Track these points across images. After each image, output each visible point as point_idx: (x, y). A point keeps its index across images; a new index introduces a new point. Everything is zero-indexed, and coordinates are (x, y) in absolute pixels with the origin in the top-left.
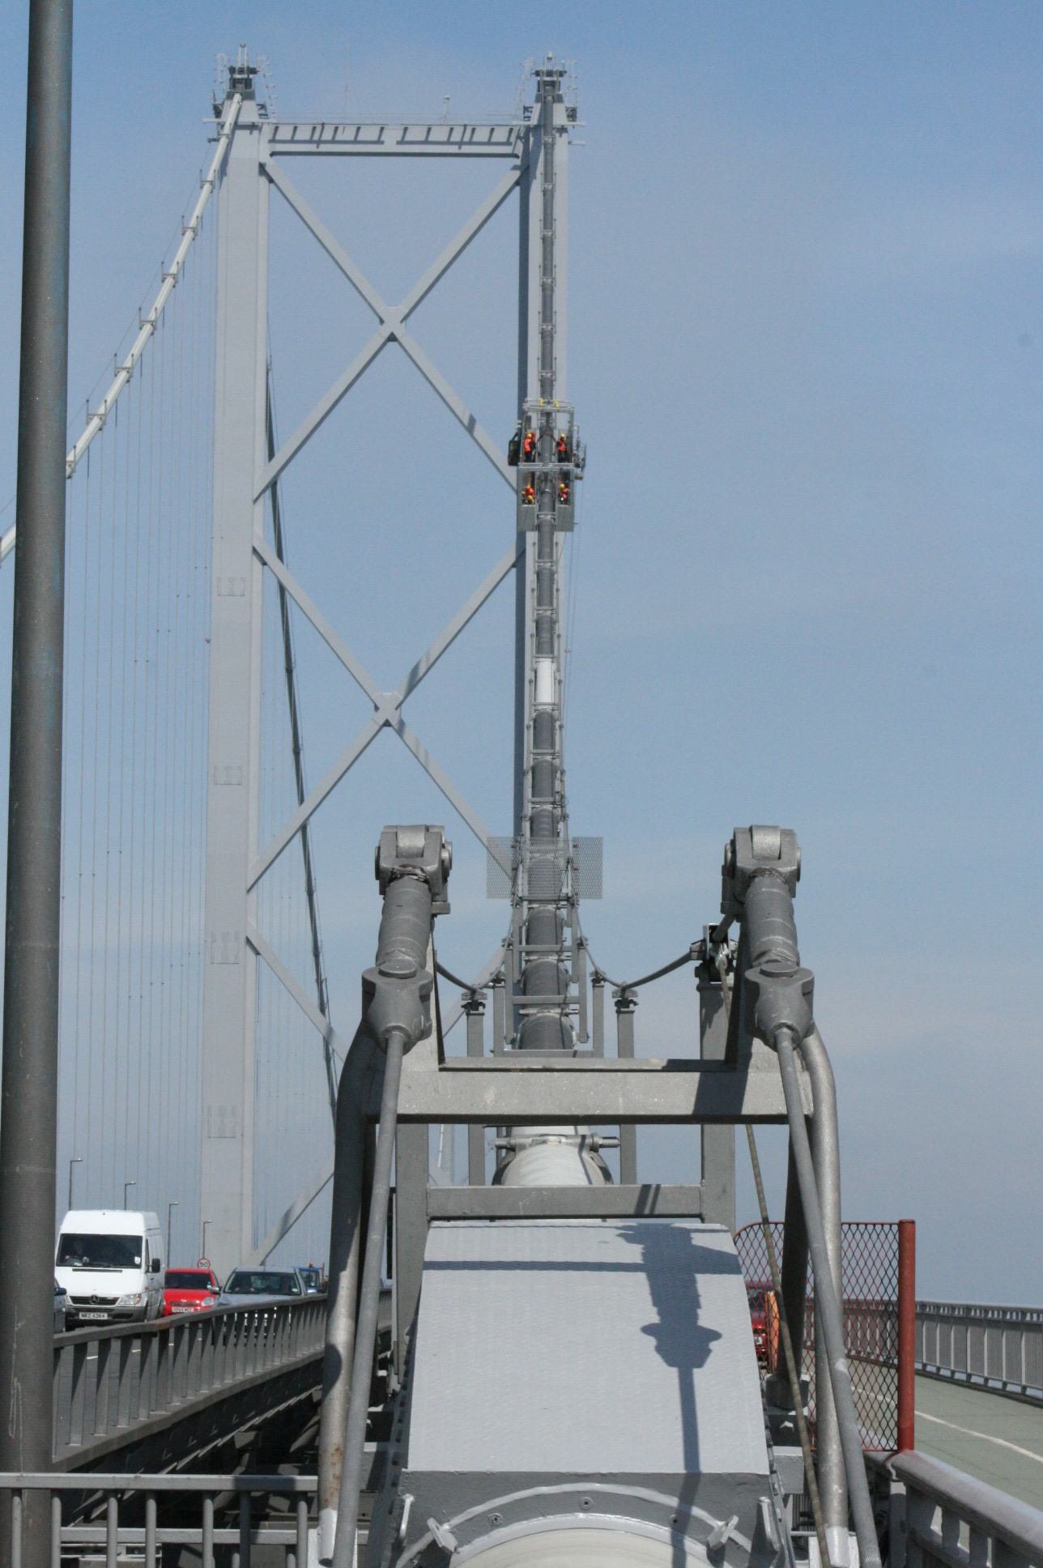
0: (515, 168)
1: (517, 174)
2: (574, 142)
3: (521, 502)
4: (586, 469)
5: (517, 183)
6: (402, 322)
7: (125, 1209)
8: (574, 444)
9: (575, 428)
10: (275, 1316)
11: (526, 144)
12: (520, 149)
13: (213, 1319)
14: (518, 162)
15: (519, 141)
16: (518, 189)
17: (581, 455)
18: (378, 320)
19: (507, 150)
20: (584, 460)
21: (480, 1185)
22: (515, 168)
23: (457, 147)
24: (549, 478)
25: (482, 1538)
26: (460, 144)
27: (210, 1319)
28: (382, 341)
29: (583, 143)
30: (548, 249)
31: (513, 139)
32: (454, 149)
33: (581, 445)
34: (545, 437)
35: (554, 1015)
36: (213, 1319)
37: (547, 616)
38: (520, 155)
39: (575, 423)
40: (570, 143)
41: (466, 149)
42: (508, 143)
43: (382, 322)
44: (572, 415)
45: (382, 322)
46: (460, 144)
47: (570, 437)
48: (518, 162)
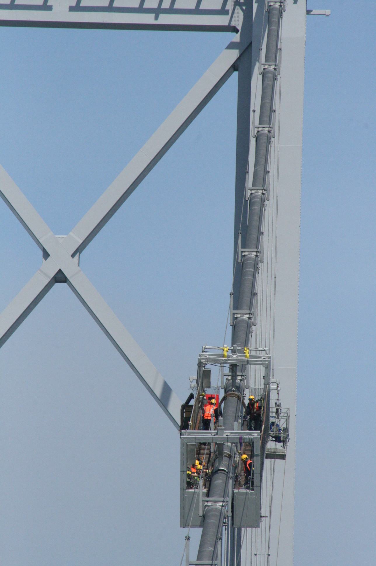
0: (232, 46)
1: (234, 54)
2: (314, 12)
3: (185, 485)
4: (289, 444)
5: (234, 67)
6: (73, 256)
7: (181, 471)
8: (273, 409)
9: (273, 386)
10: (186, 496)
11: (248, 14)
12: (238, 21)
13: (207, 443)
14: (236, 38)
15: (238, 8)
16: (236, 74)
17: (282, 424)
18: (41, 253)
19: (222, 20)
20: (286, 430)
21: (221, 436)
22: (232, 46)
23: (153, 15)
24: (226, 451)
25: (276, 127)
26: (157, 11)
27: (206, 443)
28: (47, 281)
29: (328, 12)
30: (263, 152)
31: (229, 6)
32: (148, 19)
33: (283, 410)
34: (229, 398)
35: (218, 506)
36: (207, 443)
37: (216, 510)
38: (239, 28)
39: (272, 380)
40: (308, 12)
41: (165, 19)
42: (223, 11)
43: (46, 255)
44: (267, 367)
45: (46, 255)
46: (157, 11)
47: (266, 398)
48: (236, 38)
